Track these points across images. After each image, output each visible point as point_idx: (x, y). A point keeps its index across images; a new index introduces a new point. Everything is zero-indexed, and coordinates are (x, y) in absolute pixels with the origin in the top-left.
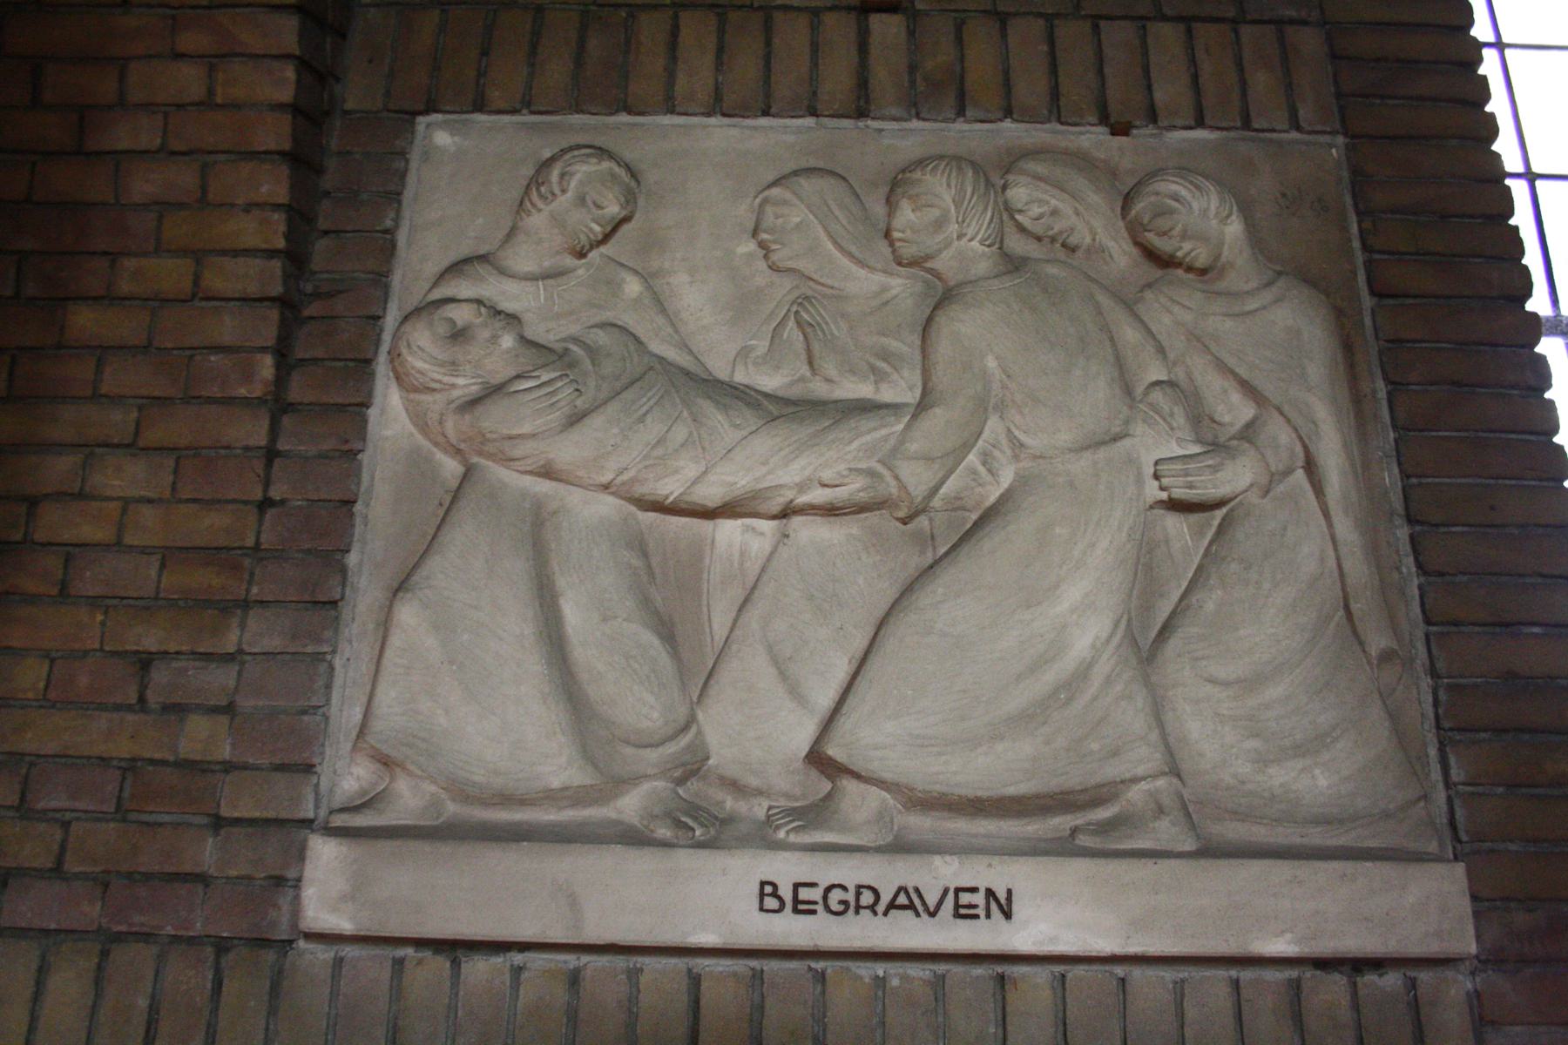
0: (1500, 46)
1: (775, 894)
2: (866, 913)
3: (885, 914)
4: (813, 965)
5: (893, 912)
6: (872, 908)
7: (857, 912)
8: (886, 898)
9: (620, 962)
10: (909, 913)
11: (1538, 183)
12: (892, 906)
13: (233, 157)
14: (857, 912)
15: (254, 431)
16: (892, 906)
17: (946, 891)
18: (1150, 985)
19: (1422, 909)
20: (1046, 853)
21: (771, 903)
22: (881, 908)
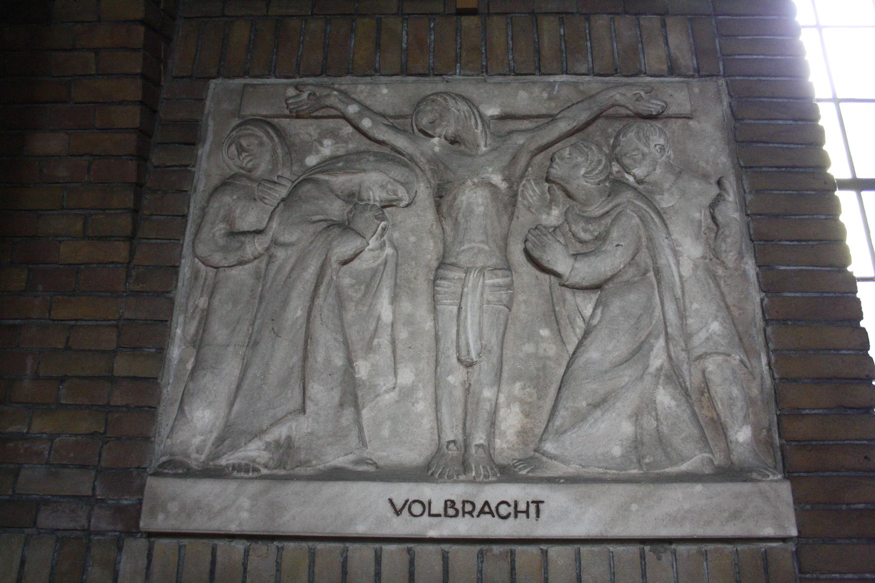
0: (819, 27)
1: (453, 507)
2: (467, 516)
3: (478, 516)
4: (542, 547)
5: (482, 516)
6: (470, 513)
7: (464, 516)
8: (479, 507)
9: (340, 545)
10: (489, 516)
11: (841, 105)
12: (482, 512)
13: (542, 121)
14: (516, 517)
15: (121, 250)
16: (482, 512)
17: (407, 501)
18: (362, 554)
19: (769, 511)
20: (319, 480)
21: (451, 512)
22: (475, 513)
